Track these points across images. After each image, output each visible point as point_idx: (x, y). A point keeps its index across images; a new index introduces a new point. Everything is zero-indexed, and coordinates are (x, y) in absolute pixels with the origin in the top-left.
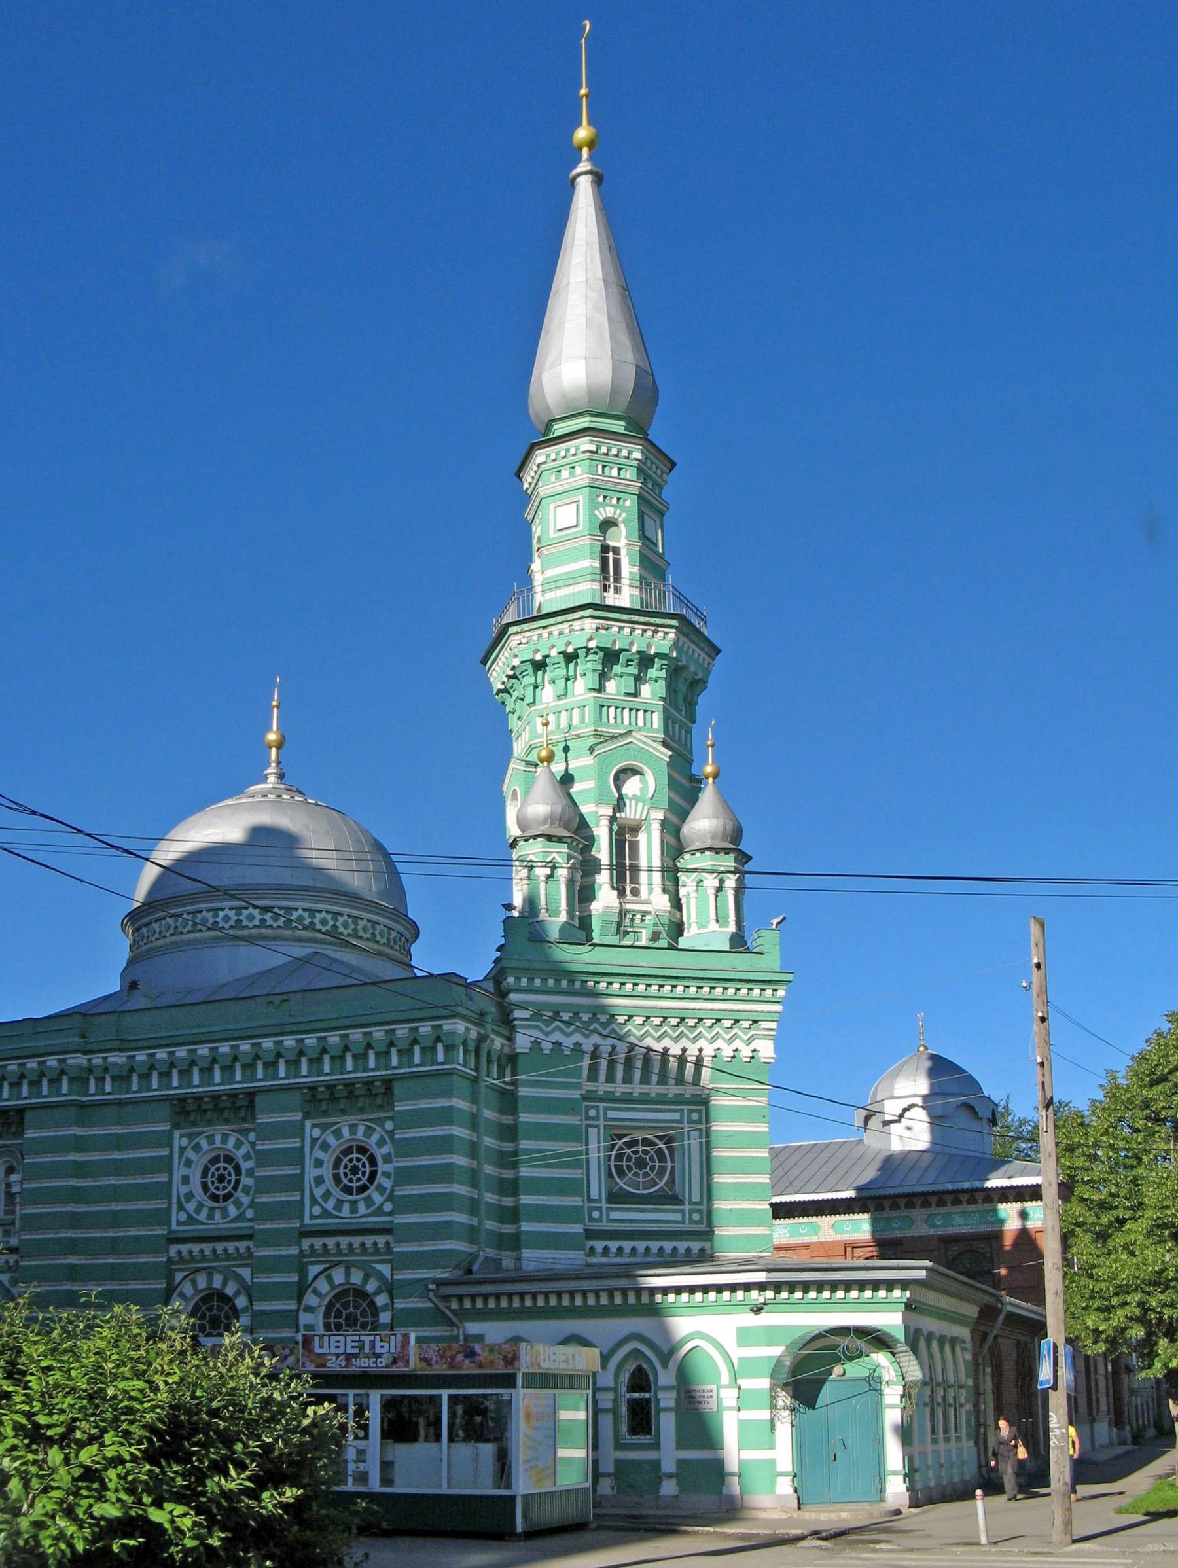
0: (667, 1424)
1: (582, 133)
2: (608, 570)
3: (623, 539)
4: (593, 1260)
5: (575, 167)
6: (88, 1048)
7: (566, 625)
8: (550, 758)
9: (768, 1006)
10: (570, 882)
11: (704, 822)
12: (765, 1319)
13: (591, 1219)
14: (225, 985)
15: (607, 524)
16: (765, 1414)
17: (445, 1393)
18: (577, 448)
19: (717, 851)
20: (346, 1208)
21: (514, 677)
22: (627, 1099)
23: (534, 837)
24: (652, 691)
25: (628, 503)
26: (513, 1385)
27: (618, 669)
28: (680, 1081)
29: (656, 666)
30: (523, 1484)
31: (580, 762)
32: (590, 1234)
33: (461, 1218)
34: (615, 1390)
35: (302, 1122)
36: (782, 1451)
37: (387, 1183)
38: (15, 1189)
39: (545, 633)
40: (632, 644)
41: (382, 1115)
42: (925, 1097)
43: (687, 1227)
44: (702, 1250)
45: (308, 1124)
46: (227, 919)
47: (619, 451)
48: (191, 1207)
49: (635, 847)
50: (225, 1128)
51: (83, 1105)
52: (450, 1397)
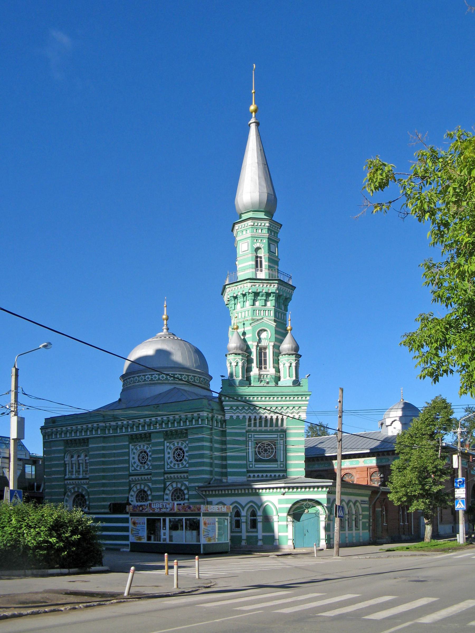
0: (260, 525)
1: (252, 108)
2: (258, 264)
3: (263, 254)
4: (249, 479)
5: (250, 120)
6: (105, 421)
7: (242, 285)
8: (237, 328)
9: (304, 402)
10: (243, 367)
11: (287, 345)
12: (286, 497)
13: (250, 467)
14: (148, 398)
15: (257, 249)
16: (285, 523)
17: (184, 518)
18: (247, 224)
19: (289, 355)
20: (176, 466)
21: (229, 301)
22: (261, 431)
23: (231, 354)
24: (271, 304)
25: (264, 241)
26: (200, 516)
27: (259, 298)
28: (277, 425)
29: (272, 296)
30: (203, 541)
31: (248, 328)
32: (248, 472)
33: (208, 468)
34: (246, 516)
35: (164, 442)
36: (289, 533)
37: (187, 458)
38: (87, 461)
39: (236, 287)
40: (263, 290)
41: (185, 439)
42: (400, 417)
43: (279, 469)
44: (283, 475)
45: (166, 442)
46: (148, 378)
47: (261, 224)
48: (135, 466)
49: (265, 354)
50: (143, 443)
51: (104, 437)
52: (186, 519)
